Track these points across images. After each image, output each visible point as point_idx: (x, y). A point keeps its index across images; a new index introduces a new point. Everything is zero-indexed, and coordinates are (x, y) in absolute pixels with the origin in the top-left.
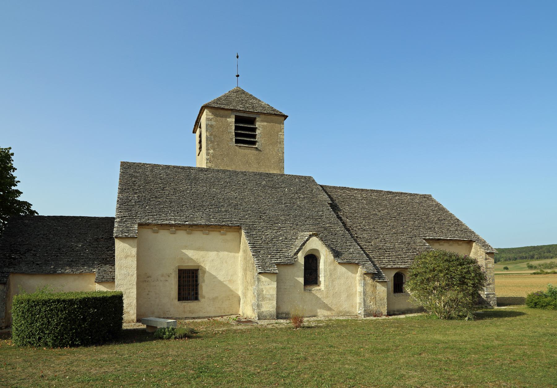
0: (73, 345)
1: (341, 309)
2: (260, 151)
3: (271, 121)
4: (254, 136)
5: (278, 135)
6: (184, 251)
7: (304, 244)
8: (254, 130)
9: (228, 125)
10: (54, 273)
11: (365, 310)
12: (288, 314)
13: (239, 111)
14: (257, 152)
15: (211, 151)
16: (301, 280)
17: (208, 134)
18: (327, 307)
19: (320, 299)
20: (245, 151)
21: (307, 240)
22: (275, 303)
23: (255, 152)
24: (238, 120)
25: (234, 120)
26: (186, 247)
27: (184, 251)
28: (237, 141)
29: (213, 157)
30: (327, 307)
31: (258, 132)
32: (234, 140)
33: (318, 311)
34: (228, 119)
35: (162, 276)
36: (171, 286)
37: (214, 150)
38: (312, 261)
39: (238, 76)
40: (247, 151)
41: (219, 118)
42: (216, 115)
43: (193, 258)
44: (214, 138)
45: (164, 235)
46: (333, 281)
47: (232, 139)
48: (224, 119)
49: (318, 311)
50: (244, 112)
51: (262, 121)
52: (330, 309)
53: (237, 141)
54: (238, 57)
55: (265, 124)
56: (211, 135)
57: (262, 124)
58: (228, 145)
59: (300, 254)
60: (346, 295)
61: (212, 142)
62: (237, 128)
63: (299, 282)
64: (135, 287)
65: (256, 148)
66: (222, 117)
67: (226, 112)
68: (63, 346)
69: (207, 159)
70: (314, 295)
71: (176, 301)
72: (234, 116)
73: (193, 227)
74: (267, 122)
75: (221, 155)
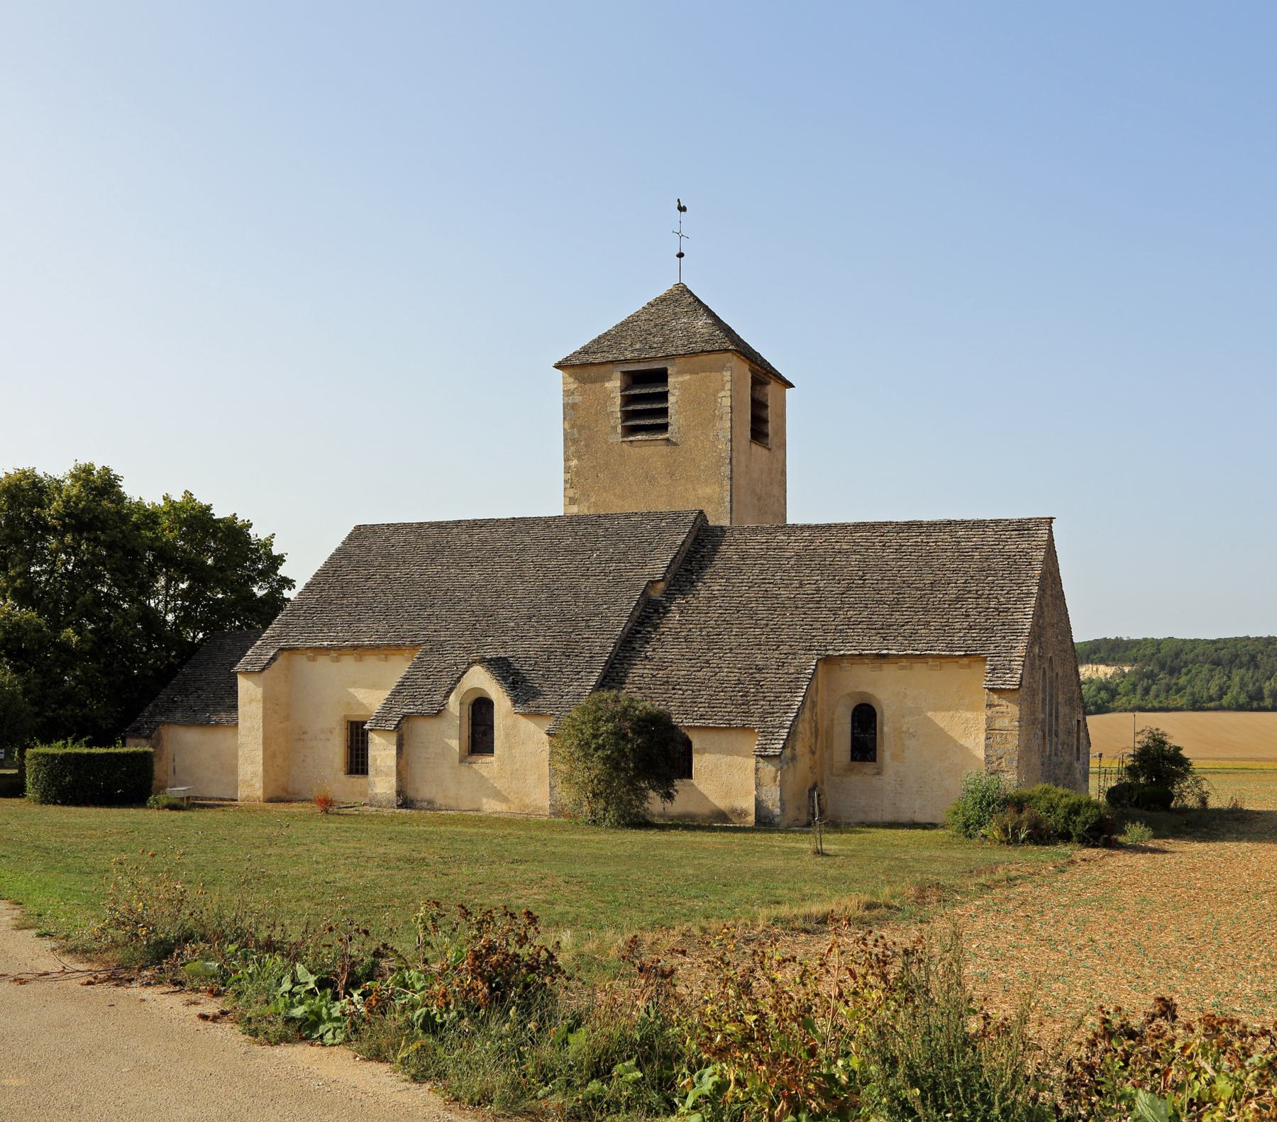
0: (55, 803)
1: (527, 801)
2: (675, 444)
3: (703, 369)
4: (664, 412)
5: (716, 401)
6: (351, 690)
7: (459, 679)
8: (664, 397)
9: (608, 397)
10: (206, 724)
11: (551, 805)
12: (430, 802)
13: (626, 361)
14: (668, 449)
15: (574, 463)
16: (455, 744)
17: (567, 426)
18: (498, 795)
19: (487, 780)
20: (647, 449)
21: (464, 673)
22: (393, 780)
23: (666, 450)
24: (634, 379)
25: (618, 383)
26: (354, 684)
27: (351, 690)
28: (630, 431)
29: (578, 473)
30: (498, 795)
31: (671, 399)
32: (619, 430)
33: (484, 801)
34: (607, 385)
35: (322, 732)
36: (335, 750)
37: (579, 458)
38: (481, 709)
39: (681, 255)
40: (647, 451)
41: (588, 386)
42: (581, 380)
43: (364, 701)
44: (579, 432)
45: (324, 662)
46: (511, 748)
47: (615, 428)
48: (598, 385)
49: (484, 801)
50: (639, 361)
51: (681, 373)
52: (505, 800)
53: (630, 431)
54: (682, 209)
55: (687, 377)
56: (572, 427)
57: (681, 379)
58: (606, 442)
59: (452, 697)
60: (536, 777)
61: (575, 441)
62: (627, 400)
63: (448, 747)
64: (261, 748)
65: (667, 440)
66: (595, 382)
67: (603, 369)
68: (48, 803)
69: (566, 482)
70: (476, 772)
71: (341, 775)
72: (618, 375)
73: (358, 650)
74: (691, 372)
75: (594, 467)
